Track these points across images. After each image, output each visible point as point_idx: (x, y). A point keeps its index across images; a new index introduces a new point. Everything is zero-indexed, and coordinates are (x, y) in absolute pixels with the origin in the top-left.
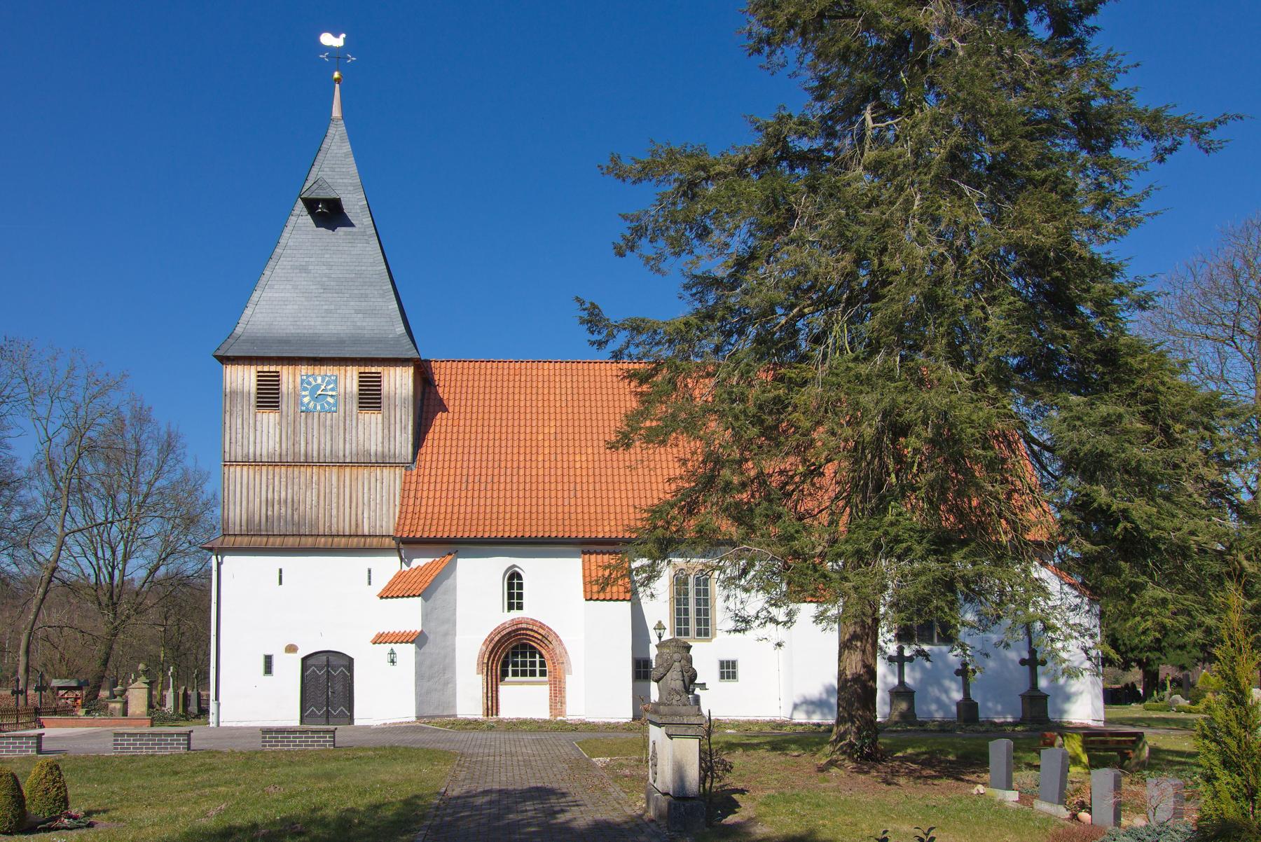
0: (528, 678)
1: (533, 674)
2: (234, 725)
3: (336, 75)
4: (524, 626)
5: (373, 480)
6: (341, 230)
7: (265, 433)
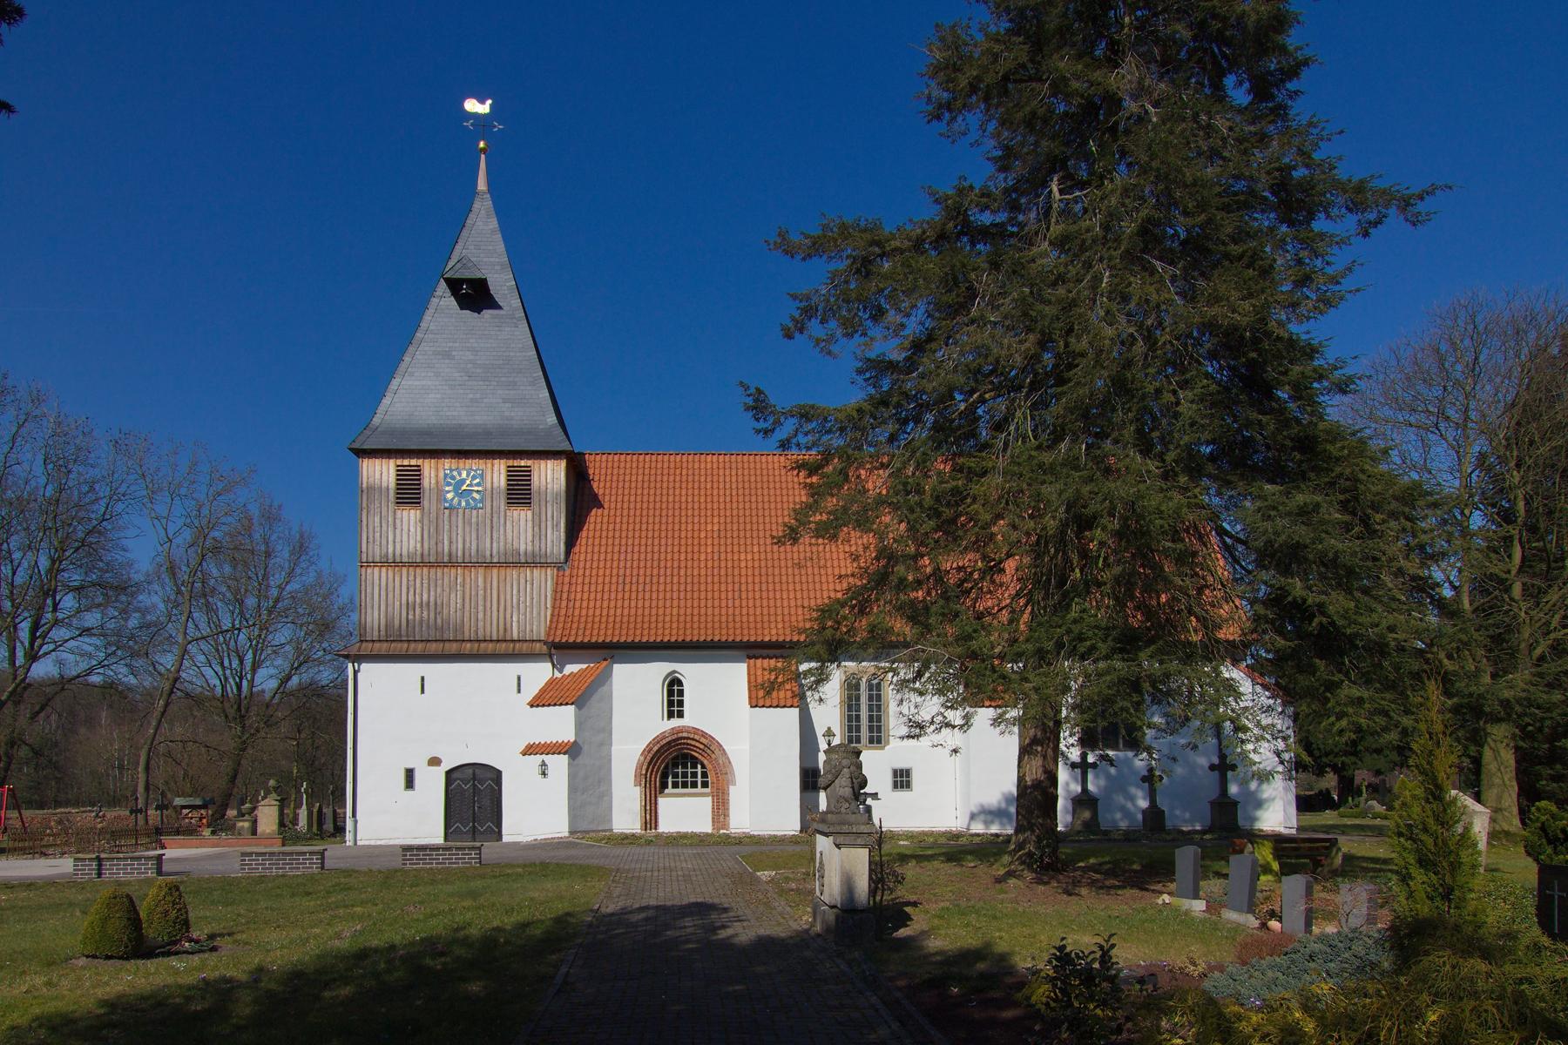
0: (680, 790)
1: (694, 785)
3: (482, 145)
7: (406, 531)
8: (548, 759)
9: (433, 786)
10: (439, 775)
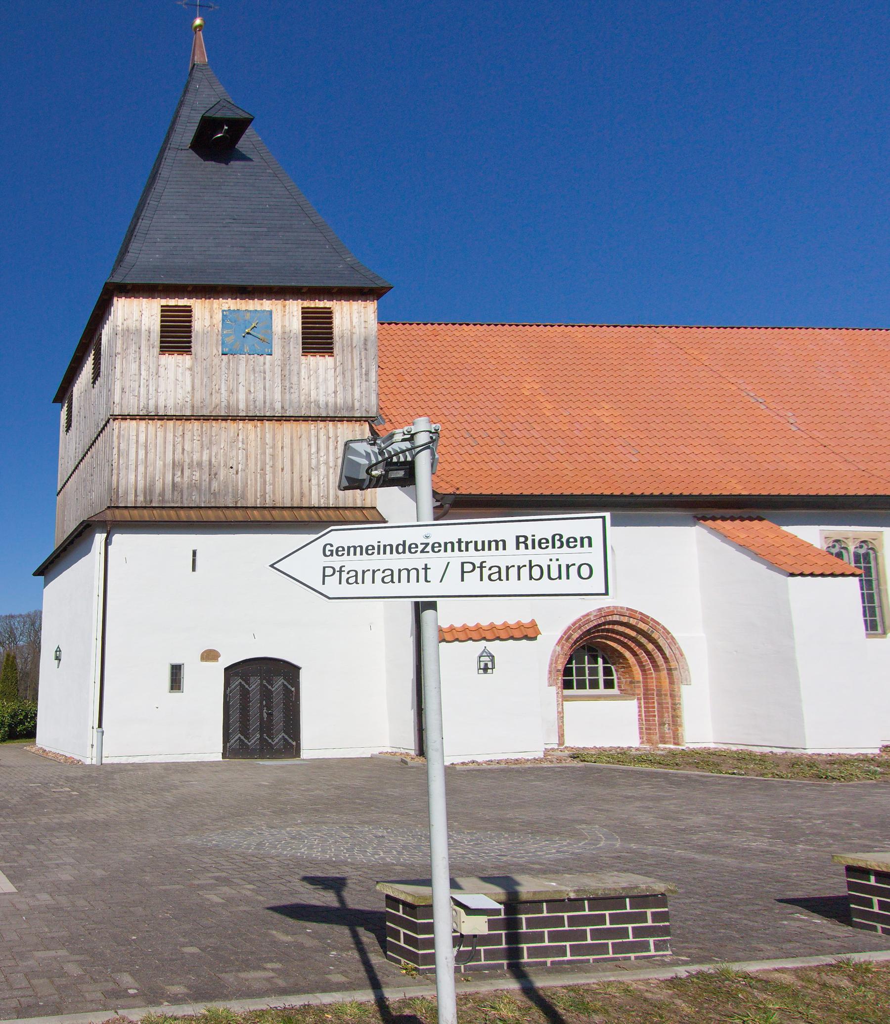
0: (588, 691)
1: (594, 685)
2: (124, 760)
3: (198, 22)
4: (616, 618)
5: (323, 438)
6: (235, 164)
7: (173, 380)
8: (494, 647)
9: (207, 691)
10: (215, 674)
